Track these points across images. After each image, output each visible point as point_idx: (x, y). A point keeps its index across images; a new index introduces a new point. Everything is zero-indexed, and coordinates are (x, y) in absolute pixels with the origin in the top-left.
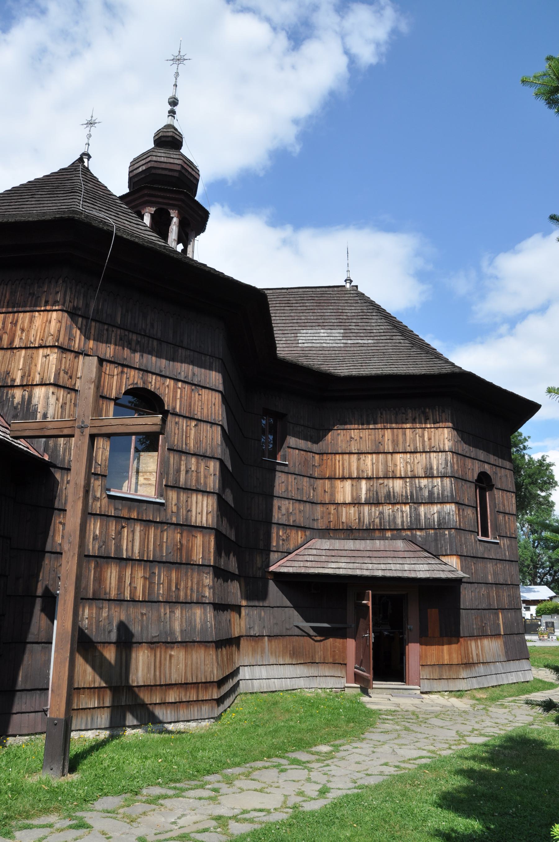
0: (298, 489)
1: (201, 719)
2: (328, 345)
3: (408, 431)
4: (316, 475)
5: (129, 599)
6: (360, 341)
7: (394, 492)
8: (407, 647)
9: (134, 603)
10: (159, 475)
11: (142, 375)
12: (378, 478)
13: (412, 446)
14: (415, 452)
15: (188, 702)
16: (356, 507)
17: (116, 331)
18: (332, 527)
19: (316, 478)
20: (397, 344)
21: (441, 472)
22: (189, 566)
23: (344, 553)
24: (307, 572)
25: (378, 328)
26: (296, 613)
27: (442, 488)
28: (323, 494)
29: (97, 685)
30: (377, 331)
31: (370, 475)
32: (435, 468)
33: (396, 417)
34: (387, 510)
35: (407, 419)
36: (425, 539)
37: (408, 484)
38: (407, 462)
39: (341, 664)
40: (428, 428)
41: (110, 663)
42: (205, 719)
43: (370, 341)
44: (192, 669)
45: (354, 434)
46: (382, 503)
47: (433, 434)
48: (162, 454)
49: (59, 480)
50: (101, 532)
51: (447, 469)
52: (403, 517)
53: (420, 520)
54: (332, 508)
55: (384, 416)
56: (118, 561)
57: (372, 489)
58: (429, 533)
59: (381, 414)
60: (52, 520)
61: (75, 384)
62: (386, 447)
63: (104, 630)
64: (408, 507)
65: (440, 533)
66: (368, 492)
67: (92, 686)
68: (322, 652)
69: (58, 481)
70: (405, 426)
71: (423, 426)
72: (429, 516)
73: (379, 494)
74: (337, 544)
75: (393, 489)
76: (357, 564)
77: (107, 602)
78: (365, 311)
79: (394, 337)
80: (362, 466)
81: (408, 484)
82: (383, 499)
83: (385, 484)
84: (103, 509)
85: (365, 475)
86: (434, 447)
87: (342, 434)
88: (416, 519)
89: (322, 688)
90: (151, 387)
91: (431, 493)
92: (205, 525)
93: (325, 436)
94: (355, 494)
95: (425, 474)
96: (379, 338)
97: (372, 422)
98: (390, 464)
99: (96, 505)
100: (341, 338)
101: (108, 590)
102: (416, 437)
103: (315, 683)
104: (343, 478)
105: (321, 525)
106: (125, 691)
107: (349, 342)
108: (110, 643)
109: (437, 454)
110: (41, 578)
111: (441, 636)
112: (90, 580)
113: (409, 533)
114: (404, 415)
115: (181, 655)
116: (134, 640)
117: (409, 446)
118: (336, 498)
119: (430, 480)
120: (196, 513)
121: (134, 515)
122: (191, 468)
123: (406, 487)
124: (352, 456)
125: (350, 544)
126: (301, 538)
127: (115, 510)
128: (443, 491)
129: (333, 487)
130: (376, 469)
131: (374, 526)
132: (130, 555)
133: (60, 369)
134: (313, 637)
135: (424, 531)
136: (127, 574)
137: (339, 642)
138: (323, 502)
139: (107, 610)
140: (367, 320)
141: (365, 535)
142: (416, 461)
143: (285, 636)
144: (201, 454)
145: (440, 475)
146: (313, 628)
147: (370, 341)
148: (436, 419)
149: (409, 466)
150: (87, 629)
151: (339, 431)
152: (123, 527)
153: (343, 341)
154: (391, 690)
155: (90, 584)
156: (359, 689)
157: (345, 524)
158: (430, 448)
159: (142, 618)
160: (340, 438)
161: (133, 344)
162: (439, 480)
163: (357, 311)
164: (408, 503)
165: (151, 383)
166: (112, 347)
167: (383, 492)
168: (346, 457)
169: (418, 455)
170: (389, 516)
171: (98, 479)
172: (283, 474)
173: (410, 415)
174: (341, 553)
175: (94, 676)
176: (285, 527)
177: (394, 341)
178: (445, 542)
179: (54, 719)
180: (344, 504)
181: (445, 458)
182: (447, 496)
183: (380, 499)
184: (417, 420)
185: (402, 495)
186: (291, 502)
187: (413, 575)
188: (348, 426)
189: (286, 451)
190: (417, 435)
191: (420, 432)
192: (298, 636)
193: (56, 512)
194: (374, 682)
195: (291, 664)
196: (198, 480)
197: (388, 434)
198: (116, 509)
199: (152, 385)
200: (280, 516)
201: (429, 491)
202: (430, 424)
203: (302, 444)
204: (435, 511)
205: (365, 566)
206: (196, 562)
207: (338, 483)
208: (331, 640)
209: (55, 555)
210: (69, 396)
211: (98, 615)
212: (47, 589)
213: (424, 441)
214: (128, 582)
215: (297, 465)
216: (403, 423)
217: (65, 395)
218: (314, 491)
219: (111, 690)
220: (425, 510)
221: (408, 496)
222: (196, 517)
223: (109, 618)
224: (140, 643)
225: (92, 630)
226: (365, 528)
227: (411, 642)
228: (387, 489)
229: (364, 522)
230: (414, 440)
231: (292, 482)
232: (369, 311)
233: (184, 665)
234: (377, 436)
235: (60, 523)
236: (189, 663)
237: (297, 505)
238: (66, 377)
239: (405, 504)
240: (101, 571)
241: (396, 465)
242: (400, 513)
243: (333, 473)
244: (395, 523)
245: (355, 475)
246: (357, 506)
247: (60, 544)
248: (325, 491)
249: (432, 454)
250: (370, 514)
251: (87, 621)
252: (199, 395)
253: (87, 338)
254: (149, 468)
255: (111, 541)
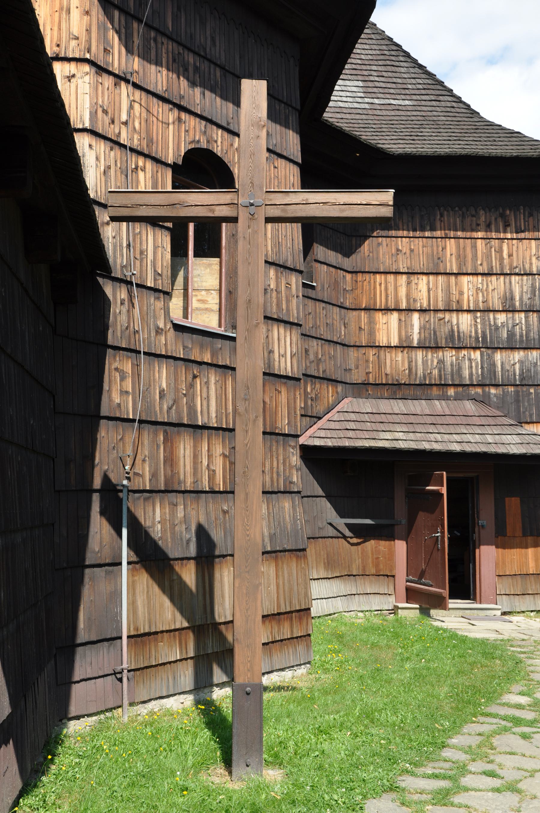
0: (327, 323)
1: (297, 665)
2: (346, 105)
3: (479, 242)
4: (347, 305)
5: (207, 489)
6: (393, 102)
7: (458, 332)
8: (477, 551)
9: (213, 495)
10: (226, 295)
11: (205, 127)
12: (436, 311)
13: (485, 264)
14: (489, 274)
15: (282, 641)
16: (405, 352)
17: (167, 44)
18: (371, 381)
19: (348, 309)
20: (449, 109)
21: (526, 304)
22: (274, 437)
23: (397, 419)
24: (353, 445)
25: (413, 81)
26: (329, 505)
27: (526, 327)
28: (357, 332)
29: (178, 626)
30: (414, 87)
31: (425, 305)
32: (517, 298)
33: (462, 221)
34: (449, 356)
35: (478, 225)
36: (503, 398)
37: (479, 320)
38: (478, 289)
39: (387, 576)
40: (508, 239)
41: (191, 591)
42: (300, 665)
43: (407, 102)
44: (284, 591)
45: (403, 244)
46: (442, 347)
47: (515, 248)
48: (227, 262)
49: (111, 298)
50: (168, 385)
51: (534, 300)
52: (471, 367)
53: (495, 372)
54: (371, 352)
55: (446, 219)
56: (191, 430)
57: (428, 326)
58: (508, 391)
59: (442, 215)
60: (105, 364)
61: (120, 133)
62: (448, 265)
63: (181, 539)
64: (478, 353)
65: (523, 391)
66: (423, 331)
67: (173, 628)
68: (360, 560)
69: (109, 300)
70: (475, 235)
71: (502, 235)
72: (508, 367)
73: (438, 333)
74: (385, 405)
75: (458, 327)
76: (420, 435)
77: (181, 495)
78: (386, 52)
79: (441, 98)
80: (414, 294)
81: (479, 320)
82: (444, 341)
83: (446, 320)
84: (169, 347)
85: (419, 305)
86: (517, 267)
87: (384, 244)
88: (489, 371)
89: (362, 611)
90: (218, 150)
91: (511, 335)
92: (290, 375)
93: (360, 247)
94: (403, 333)
95: (503, 307)
96: (418, 97)
97: (428, 228)
98: (454, 291)
99: (160, 341)
100: (362, 95)
101: (182, 477)
102: (491, 251)
103: (356, 604)
104: (387, 310)
105: (357, 377)
106: (210, 630)
107: (376, 101)
108: (189, 559)
109: (520, 277)
110: (97, 461)
111: (525, 535)
112: (160, 461)
113: (479, 390)
114: (474, 219)
115: (271, 571)
116: (217, 553)
117: (481, 264)
118: (377, 339)
119: (510, 315)
120: (279, 356)
121: (207, 358)
122: (269, 285)
123: (476, 326)
124: (399, 277)
125: (398, 406)
126: (332, 396)
127: (184, 349)
128: (528, 331)
129: (372, 322)
130: (434, 297)
131: (430, 379)
132: (206, 421)
133: (96, 103)
134: (349, 539)
135: (501, 388)
136: (203, 450)
137: (383, 545)
138: (358, 344)
139: (182, 507)
140: (394, 69)
141: (419, 392)
142: (491, 287)
143: (318, 538)
144: (281, 263)
145: (524, 309)
146: (348, 525)
147: (407, 102)
148: (520, 226)
149: (480, 295)
150: (161, 538)
151: (380, 239)
152: (195, 377)
153: (367, 100)
154: (462, 611)
155: (160, 468)
156: (418, 611)
157: (389, 377)
158: (510, 269)
159: (225, 518)
160: (382, 250)
161: (191, 69)
162: (523, 315)
163: (374, 52)
164: (479, 348)
165: (216, 142)
166: (165, 72)
167: (444, 331)
168: (391, 278)
169: (494, 278)
170: (452, 365)
171: (158, 298)
172: (310, 300)
173: (483, 218)
174: (390, 418)
175: (174, 612)
176: (314, 380)
177: (443, 104)
178: (529, 405)
179: (247, 686)
180: (388, 347)
181: (532, 284)
182: (534, 339)
183: (439, 341)
184: (493, 227)
185: (470, 337)
186: (320, 342)
187: (502, 450)
188: (393, 233)
189: (312, 267)
190: (493, 249)
191: (497, 245)
192: (332, 537)
193: (109, 351)
194: (450, 601)
195: (326, 578)
196: (279, 305)
197: (451, 245)
198: (185, 348)
199: (217, 146)
200: (308, 364)
201: (508, 331)
202: (511, 233)
203: (333, 256)
204: (517, 360)
205: (432, 437)
206: (281, 430)
207: (380, 317)
208: (373, 542)
209: (114, 422)
210: (112, 153)
211: (173, 513)
212: (106, 479)
213: (502, 259)
214: (205, 462)
215: (326, 289)
216: (472, 230)
217: (107, 152)
218: (345, 327)
219: (194, 632)
220: (502, 358)
221: (478, 338)
222: (279, 362)
223: (186, 519)
224: (224, 556)
225: (167, 540)
226: (418, 382)
227: (484, 545)
228: (450, 327)
229: (416, 374)
230: (488, 256)
231: (320, 313)
232: (393, 53)
233: (275, 587)
234: (435, 248)
235: (117, 369)
236: (281, 583)
237: (326, 346)
238: (107, 120)
239: (475, 348)
240: (172, 447)
241: (461, 293)
242: (467, 362)
243: (372, 302)
244: (460, 376)
245: (404, 306)
246: (406, 351)
247: (119, 405)
248: (360, 328)
249: (513, 277)
250: (425, 362)
251: (159, 526)
252: (275, 167)
253: (129, 51)
254: (204, 284)
255: (182, 398)
